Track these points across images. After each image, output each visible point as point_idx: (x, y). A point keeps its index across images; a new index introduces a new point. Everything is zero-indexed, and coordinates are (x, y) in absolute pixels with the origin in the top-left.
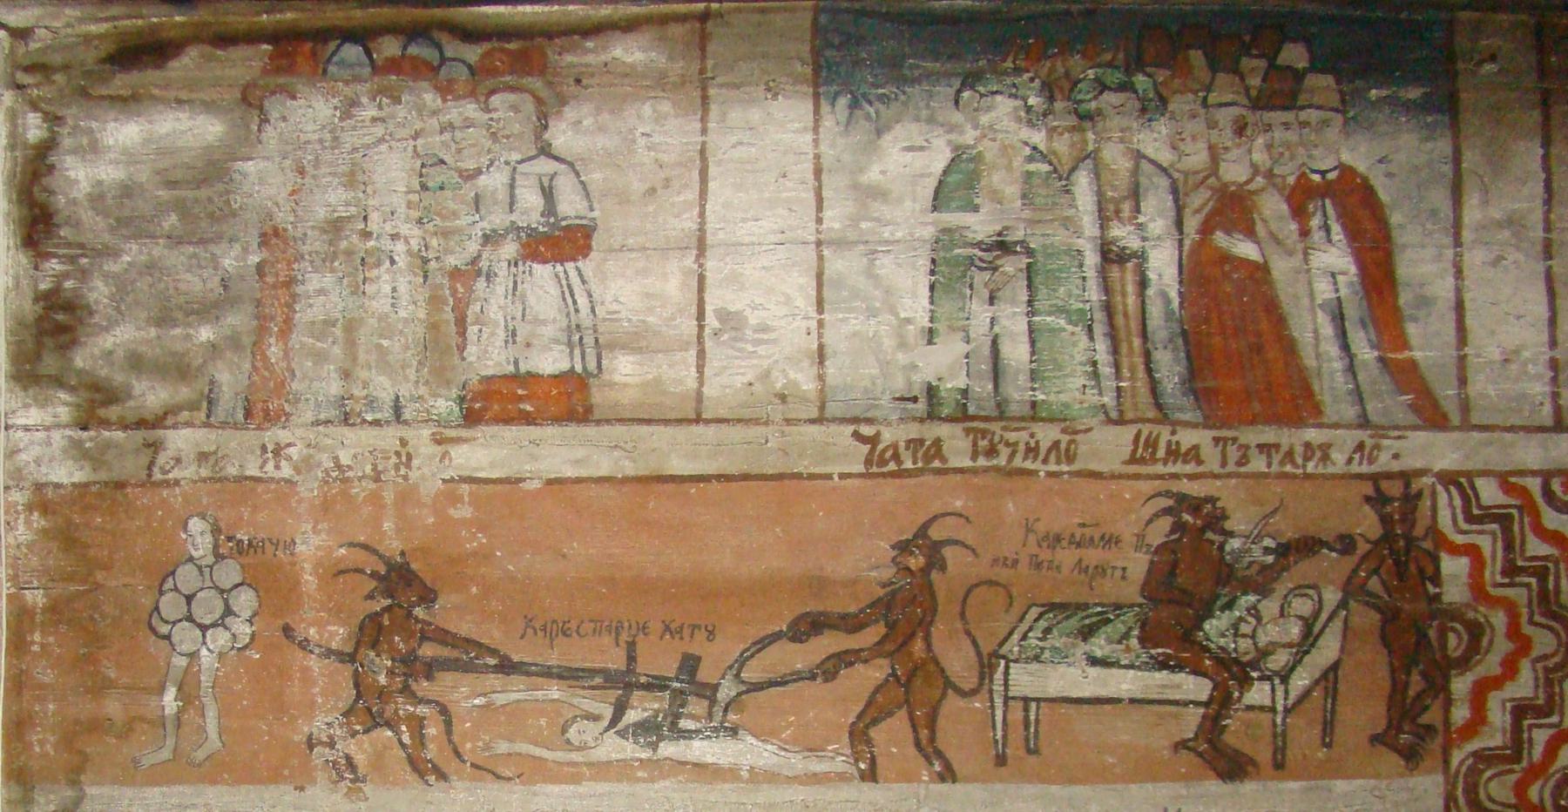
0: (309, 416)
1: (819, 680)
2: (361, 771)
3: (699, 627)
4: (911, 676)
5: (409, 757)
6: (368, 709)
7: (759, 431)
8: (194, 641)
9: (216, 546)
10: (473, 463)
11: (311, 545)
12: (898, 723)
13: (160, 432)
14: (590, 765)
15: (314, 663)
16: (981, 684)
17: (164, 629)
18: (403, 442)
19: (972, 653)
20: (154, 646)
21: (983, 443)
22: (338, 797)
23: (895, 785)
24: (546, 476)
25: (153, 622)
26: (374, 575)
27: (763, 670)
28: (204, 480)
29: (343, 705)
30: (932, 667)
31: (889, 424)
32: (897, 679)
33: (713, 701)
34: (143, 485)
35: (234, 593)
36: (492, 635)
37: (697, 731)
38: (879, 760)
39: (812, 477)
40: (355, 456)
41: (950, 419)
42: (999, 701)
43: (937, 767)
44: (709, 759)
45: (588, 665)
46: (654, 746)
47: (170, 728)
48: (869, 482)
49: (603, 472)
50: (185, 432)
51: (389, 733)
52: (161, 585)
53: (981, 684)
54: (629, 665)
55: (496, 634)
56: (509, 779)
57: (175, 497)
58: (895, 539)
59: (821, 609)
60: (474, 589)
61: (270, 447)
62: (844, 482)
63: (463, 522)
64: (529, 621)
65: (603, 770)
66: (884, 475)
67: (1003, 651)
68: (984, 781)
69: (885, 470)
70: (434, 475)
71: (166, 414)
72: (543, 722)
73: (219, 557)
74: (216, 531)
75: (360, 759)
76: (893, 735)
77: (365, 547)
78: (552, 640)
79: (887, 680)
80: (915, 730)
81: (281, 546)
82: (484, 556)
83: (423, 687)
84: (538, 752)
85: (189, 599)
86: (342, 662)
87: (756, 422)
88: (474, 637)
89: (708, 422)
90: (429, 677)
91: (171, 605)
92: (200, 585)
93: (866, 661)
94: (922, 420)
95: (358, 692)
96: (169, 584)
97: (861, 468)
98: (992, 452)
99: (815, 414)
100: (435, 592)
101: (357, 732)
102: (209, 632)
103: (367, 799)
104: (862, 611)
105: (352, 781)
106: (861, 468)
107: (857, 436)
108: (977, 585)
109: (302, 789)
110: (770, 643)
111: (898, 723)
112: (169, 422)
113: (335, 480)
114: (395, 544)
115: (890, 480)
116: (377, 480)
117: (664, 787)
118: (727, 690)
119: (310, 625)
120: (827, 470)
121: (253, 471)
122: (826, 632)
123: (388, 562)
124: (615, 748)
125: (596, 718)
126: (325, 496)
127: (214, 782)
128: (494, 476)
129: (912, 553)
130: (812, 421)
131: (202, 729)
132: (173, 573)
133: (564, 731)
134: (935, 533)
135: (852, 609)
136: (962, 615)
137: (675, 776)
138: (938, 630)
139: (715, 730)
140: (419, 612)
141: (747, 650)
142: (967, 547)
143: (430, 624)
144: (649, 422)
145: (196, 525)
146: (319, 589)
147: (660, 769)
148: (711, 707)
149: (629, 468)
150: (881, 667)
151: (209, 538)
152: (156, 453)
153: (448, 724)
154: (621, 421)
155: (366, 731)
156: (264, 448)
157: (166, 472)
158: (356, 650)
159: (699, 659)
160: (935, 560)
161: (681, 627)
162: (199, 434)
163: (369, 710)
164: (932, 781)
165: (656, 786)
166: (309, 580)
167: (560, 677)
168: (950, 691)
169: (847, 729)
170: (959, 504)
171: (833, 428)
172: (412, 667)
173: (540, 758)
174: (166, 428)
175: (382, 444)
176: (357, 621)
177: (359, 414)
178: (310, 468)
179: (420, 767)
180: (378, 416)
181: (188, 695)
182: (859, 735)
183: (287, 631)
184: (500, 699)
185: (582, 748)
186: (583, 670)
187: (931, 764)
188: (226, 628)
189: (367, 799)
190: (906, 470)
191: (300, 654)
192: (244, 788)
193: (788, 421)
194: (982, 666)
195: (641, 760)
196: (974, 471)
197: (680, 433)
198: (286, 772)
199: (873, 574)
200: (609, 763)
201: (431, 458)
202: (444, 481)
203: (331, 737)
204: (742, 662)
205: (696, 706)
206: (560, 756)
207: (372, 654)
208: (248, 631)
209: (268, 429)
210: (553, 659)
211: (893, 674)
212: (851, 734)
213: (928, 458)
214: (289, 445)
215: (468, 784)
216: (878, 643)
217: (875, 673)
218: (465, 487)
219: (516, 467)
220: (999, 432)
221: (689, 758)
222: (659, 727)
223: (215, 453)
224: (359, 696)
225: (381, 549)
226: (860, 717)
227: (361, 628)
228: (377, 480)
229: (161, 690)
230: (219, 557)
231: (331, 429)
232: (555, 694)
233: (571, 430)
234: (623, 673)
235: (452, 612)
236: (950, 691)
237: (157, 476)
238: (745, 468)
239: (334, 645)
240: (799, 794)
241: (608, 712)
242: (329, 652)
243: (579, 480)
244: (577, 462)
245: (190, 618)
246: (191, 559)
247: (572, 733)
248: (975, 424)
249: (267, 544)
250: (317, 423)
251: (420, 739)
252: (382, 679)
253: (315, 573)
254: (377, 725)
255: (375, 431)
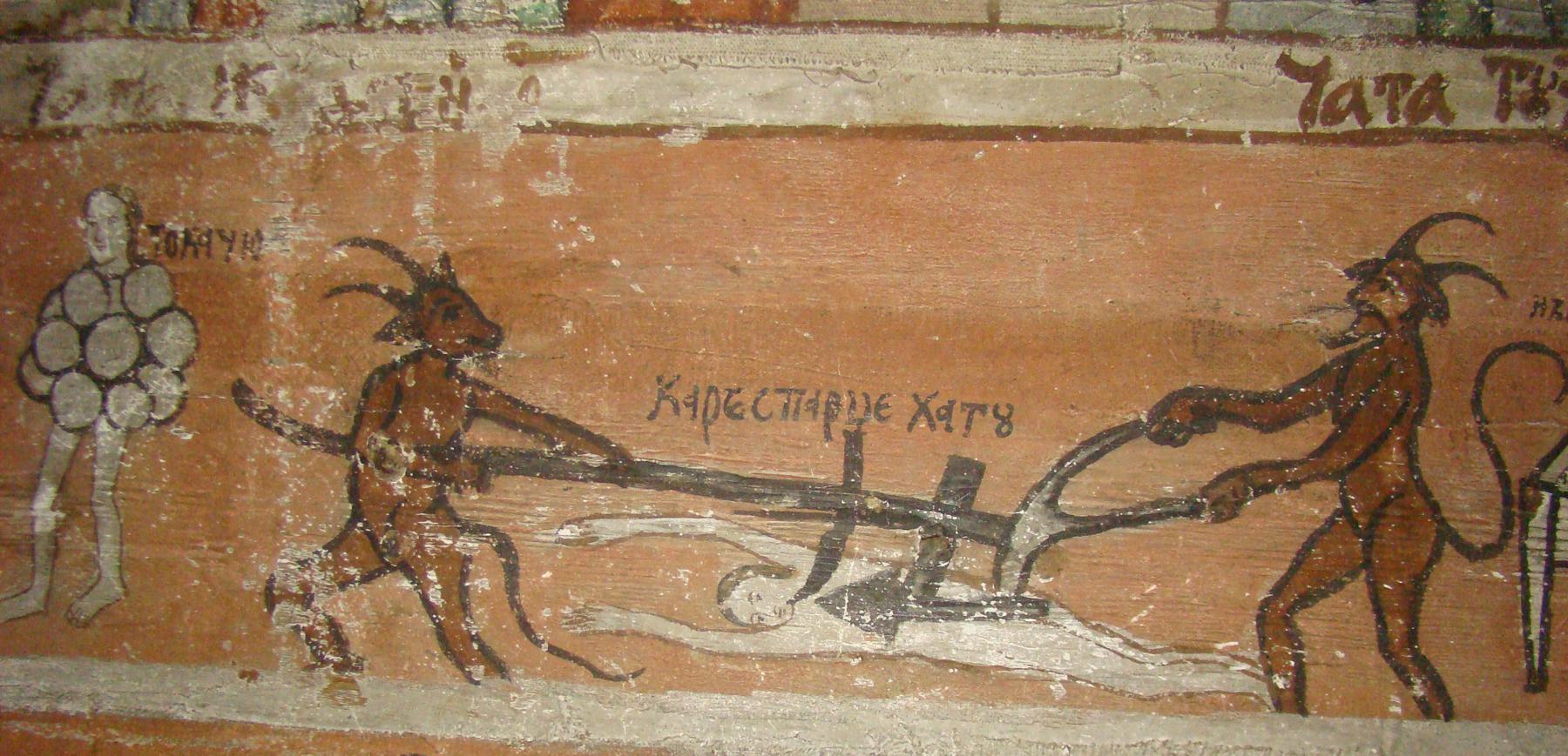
0: (297, 16)
1: (1206, 516)
2: (356, 649)
3: (982, 409)
4: (1377, 515)
5: (439, 626)
6: (371, 541)
7: (1109, 48)
8: (87, 409)
9: (132, 243)
10: (579, 99)
11: (290, 242)
12: (1351, 602)
13: (56, 47)
14: (768, 659)
15: (282, 452)
16: (1505, 536)
17: (42, 385)
18: (457, 62)
19: (1490, 477)
20: (22, 412)
21: (1520, 87)
22: (314, 694)
23: (1337, 721)
24: (707, 123)
25: (25, 370)
26: (394, 297)
27: (1101, 496)
28: (119, 129)
29: (328, 530)
30: (1417, 502)
31: (1347, 46)
32: (1352, 522)
33: (1004, 550)
34: (23, 137)
35: (156, 324)
36: (599, 411)
37: (972, 605)
38: (1312, 673)
39: (1201, 137)
40: (372, 86)
41: (1458, 42)
42: (1536, 569)
43: (1418, 691)
44: (993, 659)
45: (771, 472)
46: (889, 630)
47: (41, 556)
48: (1307, 150)
49: (811, 119)
50: (95, 46)
51: (406, 584)
52: (43, 308)
53: (1505, 536)
54: (848, 474)
55: (605, 410)
56: (619, 678)
57: (72, 158)
58: (1356, 258)
59: (1215, 382)
60: (568, 327)
61: (231, 71)
62: (1260, 150)
63: (555, 203)
64: (666, 387)
65: (791, 670)
66: (1335, 139)
67: (1549, 475)
68: (1505, 719)
69: (1338, 129)
70: (507, 119)
71: (64, 14)
72: (683, 575)
73: (136, 261)
74: (133, 215)
75: (353, 628)
76: (1338, 625)
77: (379, 245)
78: (706, 424)
79: (1331, 522)
80: (1381, 620)
81: (237, 245)
82: (590, 266)
83: (468, 502)
84: (672, 631)
85: (84, 333)
86: (332, 451)
87: (1098, 32)
88: (565, 413)
89: (1009, 29)
90: (481, 485)
91: (55, 343)
92: (101, 309)
93: (1294, 485)
94: (1407, 41)
95: (357, 506)
96: (51, 310)
97: (1291, 125)
98: (1535, 104)
99: (1209, 22)
100: (499, 330)
101: (350, 580)
102: (113, 393)
103: (363, 701)
104: (1290, 389)
105: (337, 667)
106: (1291, 125)
107: (1285, 64)
108: (1506, 349)
109: (253, 676)
110: (1116, 444)
111: (1351, 602)
112: (69, 29)
113: (338, 125)
114: (432, 242)
115: (1346, 150)
116: (409, 127)
117: (906, 707)
118: (1031, 530)
119: (280, 383)
120: (1230, 125)
121: (200, 113)
122: (1222, 426)
123: (417, 272)
124: (816, 630)
125: (784, 573)
126: (317, 157)
127: (107, 656)
128: (614, 122)
129: (1385, 286)
130: (1204, 35)
131: (91, 562)
132: (61, 289)
133: (722, 594)
134: (1430, 250)
135: (1274, 385)
136: (1476, 403)
137: (925, 688)
138: (1430, 434)
139: (1006, 603)
140: (469, 365)
141: (1072, 454)
142: (1487, 278)
143: (486, 387)
144: (901, 27)
145: (102, 205)
146: (300, 317)
147: (896, 672)
148: (999, 561)
149: (862, 112)
150: (1321, 498)
151: (121, 228)
152: (46, 82)
153: (512, 571)
154: (850, 24)
155: (367, 578)
156: (221, 73)
157: (59, 115)
158: (356, 430)
159: (980, 470)
160: (1427, 297)
161: (949, 408)
162: (117, 50)
163: (373, 538)
164: (1407, 715)
165: (890, 705)
166: (282, 303)
167: (719, 493)
168: (1448, 548)
169: (1254, 612)
170: (1473, 197)
171: (1244, 49)
172: (447, 462)
173: (677, 644)
174: (66, 39)
175: (417, 64)
176: (359, 381)
177: (382, 12)
178: (294, 107)
179: (460, 649)
180: (415, 14)
181: (73, 502)
182: (1276, 623)
183: (240, 391)
184: (608, 529)
185: (756, 627)
186: (763, 482)
187: (1409, 684)
188: (142, 386)
189: (363, 701)
190: (1378, 132)
191: (260, 435)
192: (156, 670)
193: (1160, 34)
194: (1507, 500)
195: (863, 655)
196: (1502, 139)
197: (957, 48)
198: (227, 645)
199: (1314, 321)
200: (804, 656)
201: (504, 88)
202: (525, 130)
203: (305, 586)
204: (1061, 478)
205: (972, 557)
206: (714, 640)
207: (382, 439)
208: (176, 391)
209: (230, 39)
210: (707, 461)
211: (1345, 512)
212: (1262, 620)
213: (1417, 112)
214: (262, 67)
215: (541, 684)
216: (1318, 453)
217: (1314, 505)
218: (562, 140)
219: (654, 106)
220: (1550, 67)
221: (954, 655)
222: (899, 593)
223: (141, 82)
224: (356, 516)
225: (408, 250)
226: (1278, 590)
227: (366, 393)
228: (409, 127)
229: (32, 492)
230: (136, 261)
231: (332, 38)
232: (708, 525)
233: (757, 39)
234: (835, 490)
235: (526, 368)
236: (1448, 548)
237: (47, 122)
238: (1078, 117)
239: (318, 422)
240: (1157, 730)
241: (805, 562)
242: (308, 434)
243: (767, 132)
244: (767, 97)
245: (83, 367)
246: (91, 265)
247: (737, 599)
248: (1505, 52)
249: (216, 239)
250: (309, 28)
251: (460, 597)
252: (399, 485)
253: (291, 291)
254: (385, 568)
255: (408, 41)
